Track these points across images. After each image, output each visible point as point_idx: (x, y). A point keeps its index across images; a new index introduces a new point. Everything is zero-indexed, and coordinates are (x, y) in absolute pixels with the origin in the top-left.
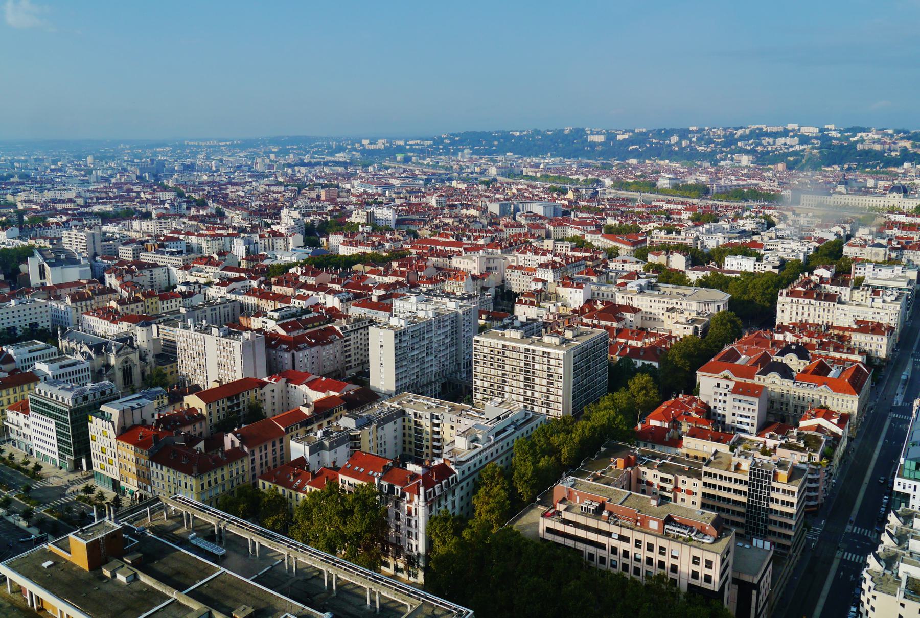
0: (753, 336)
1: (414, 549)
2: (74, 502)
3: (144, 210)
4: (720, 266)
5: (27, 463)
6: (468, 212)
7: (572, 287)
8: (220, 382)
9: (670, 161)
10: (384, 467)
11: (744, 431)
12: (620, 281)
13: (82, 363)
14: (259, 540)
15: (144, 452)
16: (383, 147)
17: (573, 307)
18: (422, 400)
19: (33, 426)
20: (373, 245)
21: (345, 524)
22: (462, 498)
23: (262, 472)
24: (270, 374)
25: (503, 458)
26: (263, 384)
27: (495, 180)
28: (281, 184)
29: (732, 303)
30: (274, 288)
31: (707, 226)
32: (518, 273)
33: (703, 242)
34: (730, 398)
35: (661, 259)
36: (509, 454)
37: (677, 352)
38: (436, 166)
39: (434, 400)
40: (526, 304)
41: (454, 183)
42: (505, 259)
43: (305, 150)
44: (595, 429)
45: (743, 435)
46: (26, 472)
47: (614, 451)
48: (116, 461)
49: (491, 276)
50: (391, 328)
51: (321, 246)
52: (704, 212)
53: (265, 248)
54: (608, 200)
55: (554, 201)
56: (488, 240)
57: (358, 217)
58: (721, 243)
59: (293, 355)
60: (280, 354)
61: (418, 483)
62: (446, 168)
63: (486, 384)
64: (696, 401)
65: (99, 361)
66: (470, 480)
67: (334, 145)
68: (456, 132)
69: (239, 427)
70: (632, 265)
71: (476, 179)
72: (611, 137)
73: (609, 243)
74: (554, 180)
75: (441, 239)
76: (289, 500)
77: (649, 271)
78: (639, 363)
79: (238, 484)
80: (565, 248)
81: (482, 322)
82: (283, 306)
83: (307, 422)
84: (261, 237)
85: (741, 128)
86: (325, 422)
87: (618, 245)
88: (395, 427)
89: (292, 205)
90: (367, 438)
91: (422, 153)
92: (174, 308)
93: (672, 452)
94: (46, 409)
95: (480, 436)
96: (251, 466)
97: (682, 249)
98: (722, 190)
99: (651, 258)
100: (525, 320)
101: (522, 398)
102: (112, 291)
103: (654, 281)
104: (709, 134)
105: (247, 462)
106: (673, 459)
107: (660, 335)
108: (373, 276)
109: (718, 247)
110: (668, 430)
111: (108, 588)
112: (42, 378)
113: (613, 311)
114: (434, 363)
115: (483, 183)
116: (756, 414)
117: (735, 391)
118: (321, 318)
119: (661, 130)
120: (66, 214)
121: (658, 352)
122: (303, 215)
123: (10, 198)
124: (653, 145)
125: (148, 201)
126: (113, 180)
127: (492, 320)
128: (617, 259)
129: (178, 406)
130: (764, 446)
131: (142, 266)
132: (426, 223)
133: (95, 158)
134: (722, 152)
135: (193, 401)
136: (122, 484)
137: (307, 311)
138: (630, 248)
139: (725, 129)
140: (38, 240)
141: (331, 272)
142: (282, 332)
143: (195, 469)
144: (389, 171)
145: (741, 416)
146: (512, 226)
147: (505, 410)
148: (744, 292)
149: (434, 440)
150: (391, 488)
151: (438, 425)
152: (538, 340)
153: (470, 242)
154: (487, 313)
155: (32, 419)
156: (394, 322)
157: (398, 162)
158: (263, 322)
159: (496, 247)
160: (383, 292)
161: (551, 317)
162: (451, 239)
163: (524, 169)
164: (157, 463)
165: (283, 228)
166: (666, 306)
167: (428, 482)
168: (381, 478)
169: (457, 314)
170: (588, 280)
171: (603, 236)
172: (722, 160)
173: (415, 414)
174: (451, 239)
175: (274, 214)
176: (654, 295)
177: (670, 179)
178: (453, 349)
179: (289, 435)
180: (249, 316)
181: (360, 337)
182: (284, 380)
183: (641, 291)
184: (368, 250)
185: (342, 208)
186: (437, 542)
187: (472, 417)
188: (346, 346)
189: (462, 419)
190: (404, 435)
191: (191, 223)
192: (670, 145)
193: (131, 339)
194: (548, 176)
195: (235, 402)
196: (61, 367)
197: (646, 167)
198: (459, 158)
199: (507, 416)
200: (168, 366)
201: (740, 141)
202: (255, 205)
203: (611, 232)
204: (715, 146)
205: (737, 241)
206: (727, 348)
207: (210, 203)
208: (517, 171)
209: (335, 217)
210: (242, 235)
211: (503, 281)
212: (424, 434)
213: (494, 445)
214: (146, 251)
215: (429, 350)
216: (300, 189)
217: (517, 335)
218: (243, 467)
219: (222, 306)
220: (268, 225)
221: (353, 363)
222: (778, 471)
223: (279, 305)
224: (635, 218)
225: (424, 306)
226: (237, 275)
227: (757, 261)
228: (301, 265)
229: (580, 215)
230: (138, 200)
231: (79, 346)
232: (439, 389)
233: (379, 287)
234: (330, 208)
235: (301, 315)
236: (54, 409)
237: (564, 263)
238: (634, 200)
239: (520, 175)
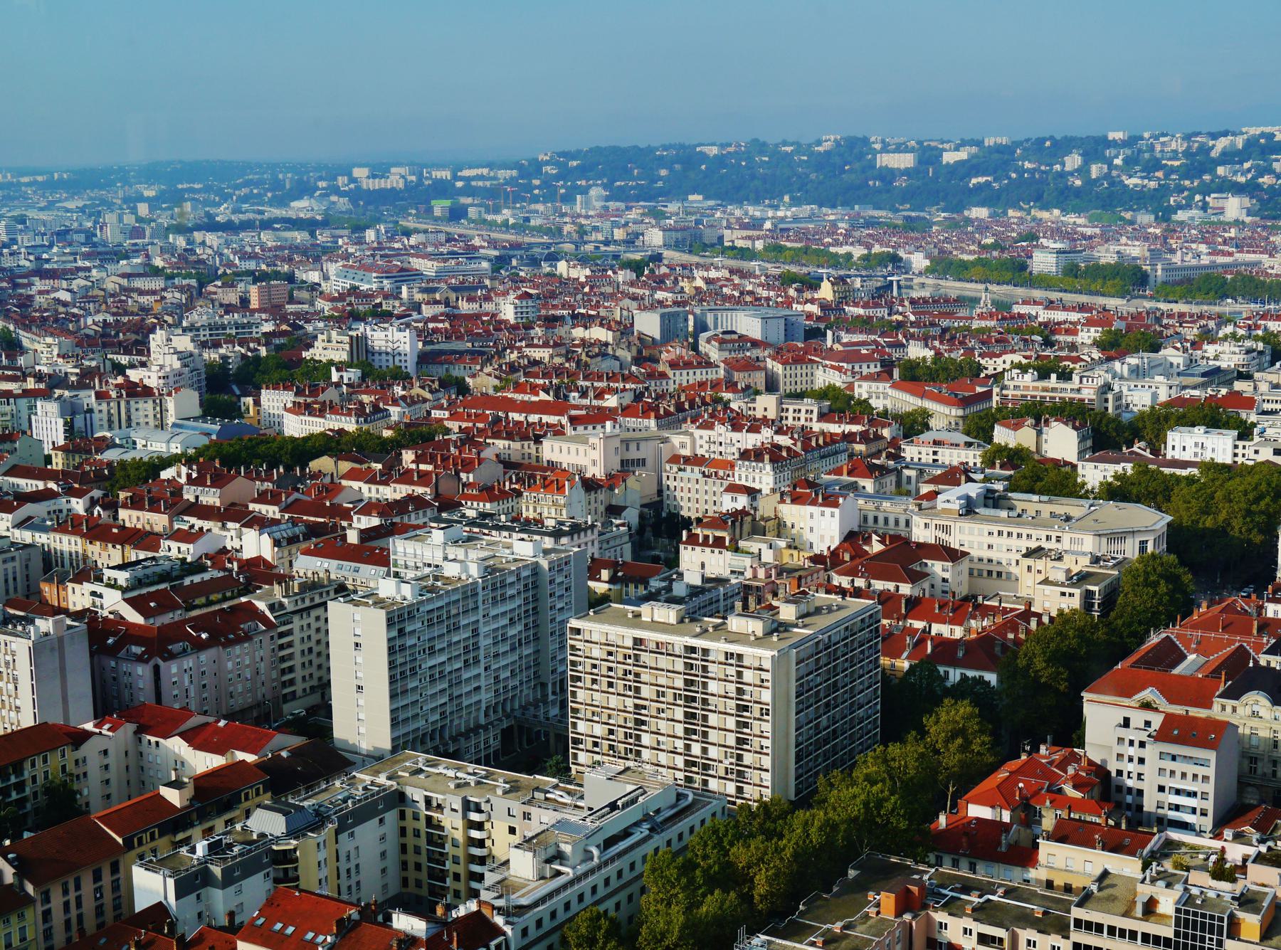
0: (1217, 608)
4: (1156, 452)
7: (814, 503)
9: (1065, 211)
10: (340, 922)
11: (1184, 826)
12: (925, 489)
16: (401, 185)
17: (817, 551)
18: (446, 769)
20: (360, 412)
23: (69, 940)
24: (100, 714)
25: (622, 896)
26: (81, 738)
27: (657, 258)
28: (157, 272)
29: (1176, 537)
30: (123, 514)
31: (1133, 360)
32: (693, 473)
33: (1119, 397)
34: (1151, 752)
35: (1023, 437)
36: (635, 888)
37: (1038, 650)
38: (523, 226)
39: (471, 767)
40: (705, 543)
41: (562, 267)
42: (665, 440)
44: (834, 827)
45: (1175, 835)
47: (878, 876)
49: (631, 481)
50: (380, 603)
51: (241, 416)
52: (1129, 328)
53: (110, 422)
54: (913, 302)
55: (789, 305)
56: (628, 399)
57: (329, 348)
58: (1163, 397)
59: (157, 669)
60: (125, 667)
63: (599, 730)
64: (1076, 758)
67: (288, 179)
69: (16, 837)
70: (955, 452)
71: (616, 257)
72: (928, 156)
73: (906, 402)
74: (797, 257)
75: (519, 397)
77: (993, 466)
78: (955, 675)
80: (805, 414)
81: (600, 587)
82: (142, 555)
83: (176, 823)
84: (100, 396)
85: (1225, 134)
86: (219, 824)
87: (929, 405)
88: (383, 830)
89: (178, 324)
90: (314, 856)
91: (494, 196)
93: (1014, 876)
95: (567, 849)
96: (41, 928)
97: (1072, 413)
98: (1178, 276)
99: (1002, 435)
100: (698, 582)
101: (680, 761)
103: (999, 486)
104: (1152, 148)
105: (32, 916)
106: (1009, 893)
107: (1005, 611)
108: (356, 485)
109: (1152, 407)
110: (1005, 827)
113: (905, 556)
114: (483, 683)
116: (1210, 788)
117: (1163, 735)
118: (226, 585)
119: (1043, 140)
121: (997, 649)
124: (1021, 174)
127: (625, 581)
128: (922, 437)
130: (1222, 859)
132: (489, 360)
134: (1180, 190)
137: (197, 567)
138: (956, 412)
139: (1188, 138)
141: (259, 478)
144: (413, 240)
145: (1178, 792)
146: (688, 365)
147: (630, 788)
148: (1206, 511)
151: (479, 826)
152: (716, 627)
153: (586, 402)
154: (613, 565)
156: (387, 588)
157: (436, 219)
158: (94, 594)
159: (645, 414)
160: (375, 521)
161: (761, 573)
162: (543, 396)
163: (727, 233)
165: (154, 376)
166: (1024, 544)
169: (536, 568)
170: (854, 487)
171: (894, 386)
172: (1180, 207)
173: (428, 801)
174: (543, 396)
175: (137, 342)
176: (997, 520)
177: (1059, 252)
178: (527, 651)
180: (61, 582)
182: (130, 728)
183: (969, 509)
184: (350, 425)
185: (296, 327)
187: (557, 806)
188: (282, 647)
190: (404, 848)
192: (1063, 175)
194: (779, 249)
195: (13, 779)
197: (1007, 225)
198: (578, 209)
199: (634, 801)
201: (1223, 163)
202: (92, 322)
203: (913, 376)
204: (1167, 176)
205: (1196, 393)
206: (1154, 639)
208: (709, 236)
209: (279, 348)
210: (58, 392)
211: (660, 492)
212: (448, 848)
213: (599, 867)
215: (470, 654)
216: (202, 285)
217: (668, 614)
218: (23, 929)
220: (119, 369)
221: (299, 687)
222: (1241, 915)
223: (133, 555)
224: (972, 343)
225: (459, 553)
226: (41, 485)
227: (1240, 437)
228: (189, 461)
229: (846, 338)
232: (495, 744)
233: (368, 509)
234: (268, 327)
235: (182, 577)
237: (798, 448)
238: (976, 300)
239: (718, 246)
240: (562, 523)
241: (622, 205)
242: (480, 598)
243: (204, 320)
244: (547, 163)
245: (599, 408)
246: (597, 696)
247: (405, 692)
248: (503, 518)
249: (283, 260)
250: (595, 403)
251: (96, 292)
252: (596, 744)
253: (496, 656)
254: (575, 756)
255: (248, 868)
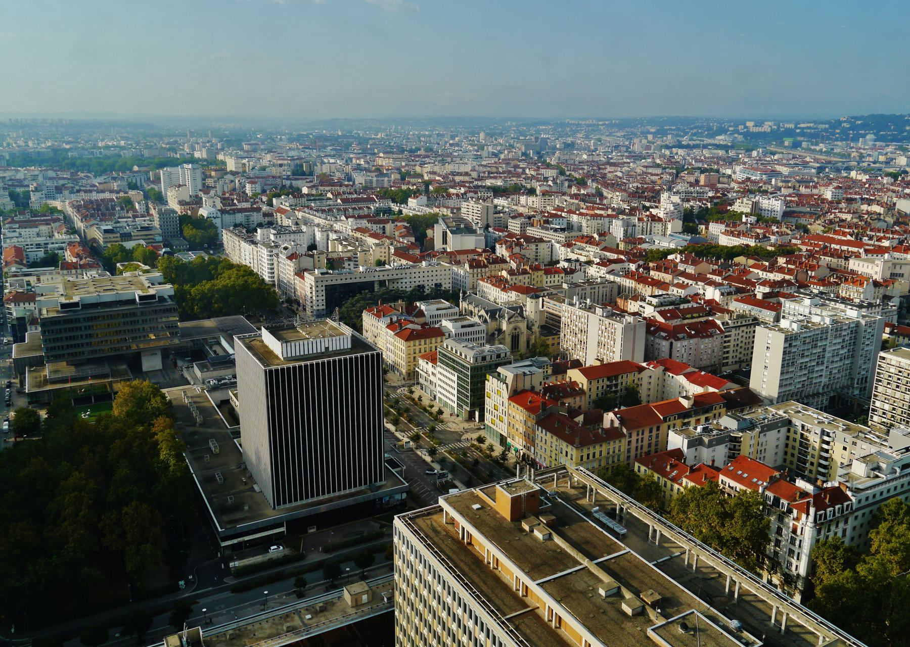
1: (793, 568)
2: (468, 448)
3: (529, 186)
5: (432, 406)
6: (869, 209)
8: (602, 361)
10: (771, 478)
13: (479, 325)
14: (659, 528)
15: (532, 416)
18: (812, 412)
19: (439, 376)
20: (757, 236)
21: (723, 525)
22: (854, 528)
28: (658, 166)
30: (652, 273)
38: (829, 153)
39: (825, 415)
41: (853, 174)
43: (684, 131)
46: (431, 414)
48: (506, 419)
49: (896, 284)
50: (781, 330)
51: (699, 234)
56: (895, 242)
57: (742, 206)
59: (671, 344)
60: (657, 341)
61: (808, 503)
62: (842, 156)
63: (887, 407)
65: (493, 325)
66: (867, 510)
67: (715, 126)
68: (860, 114)
71: (880, 170)
76: (663, 488)
79: (613, 462)
84: (639, 220)
86: (703, 418)
91: (815, 137)
92: (556, 283)
94: (452, 363)
95: (884, 466)
96: (627, 447)
102: (503, 261)
105: (624, 441)
108: (756, 271)
111: (526, 540)
112: (447, 334)
114: (824, 373)
115: (889, 175)
118: (700, 310)
120: (464, 186)
122: (683, 200)
123: (418, 169)
125: (533, 177)
126: (502, 156)
127: (898, 335)
129: (560, 377)
131: (529, 240)
132: (818, 218)
133: (487, 135)
135: (575, 375)
136: (509, 440)
137: (685, 300)
140: (442, 209)
141: (712, 263)
142: (660, 319)
143: (577, 440)
149: (821, 457)
150: (776, 501)
151: (828, 443)
153: (872, 242)
154: (892, 326)
155: (439, 369)
157: (785, 147)
160: (767, 290)
162: (849, 237)
164: (542, 428)
165: (662, 213)
167: (819, 503)
168: (766, 488)
169: (858, 324)
174: (849, 237)
175: (652, 197)
179: (666, 425)
180: (626, 299)
181: (741, 334)
182: (662, 368)
184: (752, 243)
186: (822, 568)
187: (872, 442)
188: (725, 342)
189: (859, 442)
191: (572, 201)
193: (521, 308)
196: (463, 327)
198: (860, 145)
200: (550, 338)
202: (632, 186)
207: (589, 182)
209: (716, 204)
210: (621, 217)
212: (810, 450)
213: (900, 477)
214: (532, 225)
216: (678, 173)
219: (601, 286)
220: (647, 209)
221: (730, 360)
223: (658, 292)
225: (818, 311)
228: (681, 253)
230: (524, 176)
231: (477, 309)
233: (764, 283)
234: (711, 194)
235: (679, 304)
236: (458, 363)
240: (863, 302)
241: (883, 144)
242: (829, 334)
243: (683, 189)
244: (845, 122)
245: (880, 246)
246: (889, 391)
247: (787, 372)
248: (832, 295)
249: (715, 163)
250: (876, 243)
251: (633, 173)
252: (884, 413)
253: (832, 362)
254: (872, 417)
255: (719, 441)
